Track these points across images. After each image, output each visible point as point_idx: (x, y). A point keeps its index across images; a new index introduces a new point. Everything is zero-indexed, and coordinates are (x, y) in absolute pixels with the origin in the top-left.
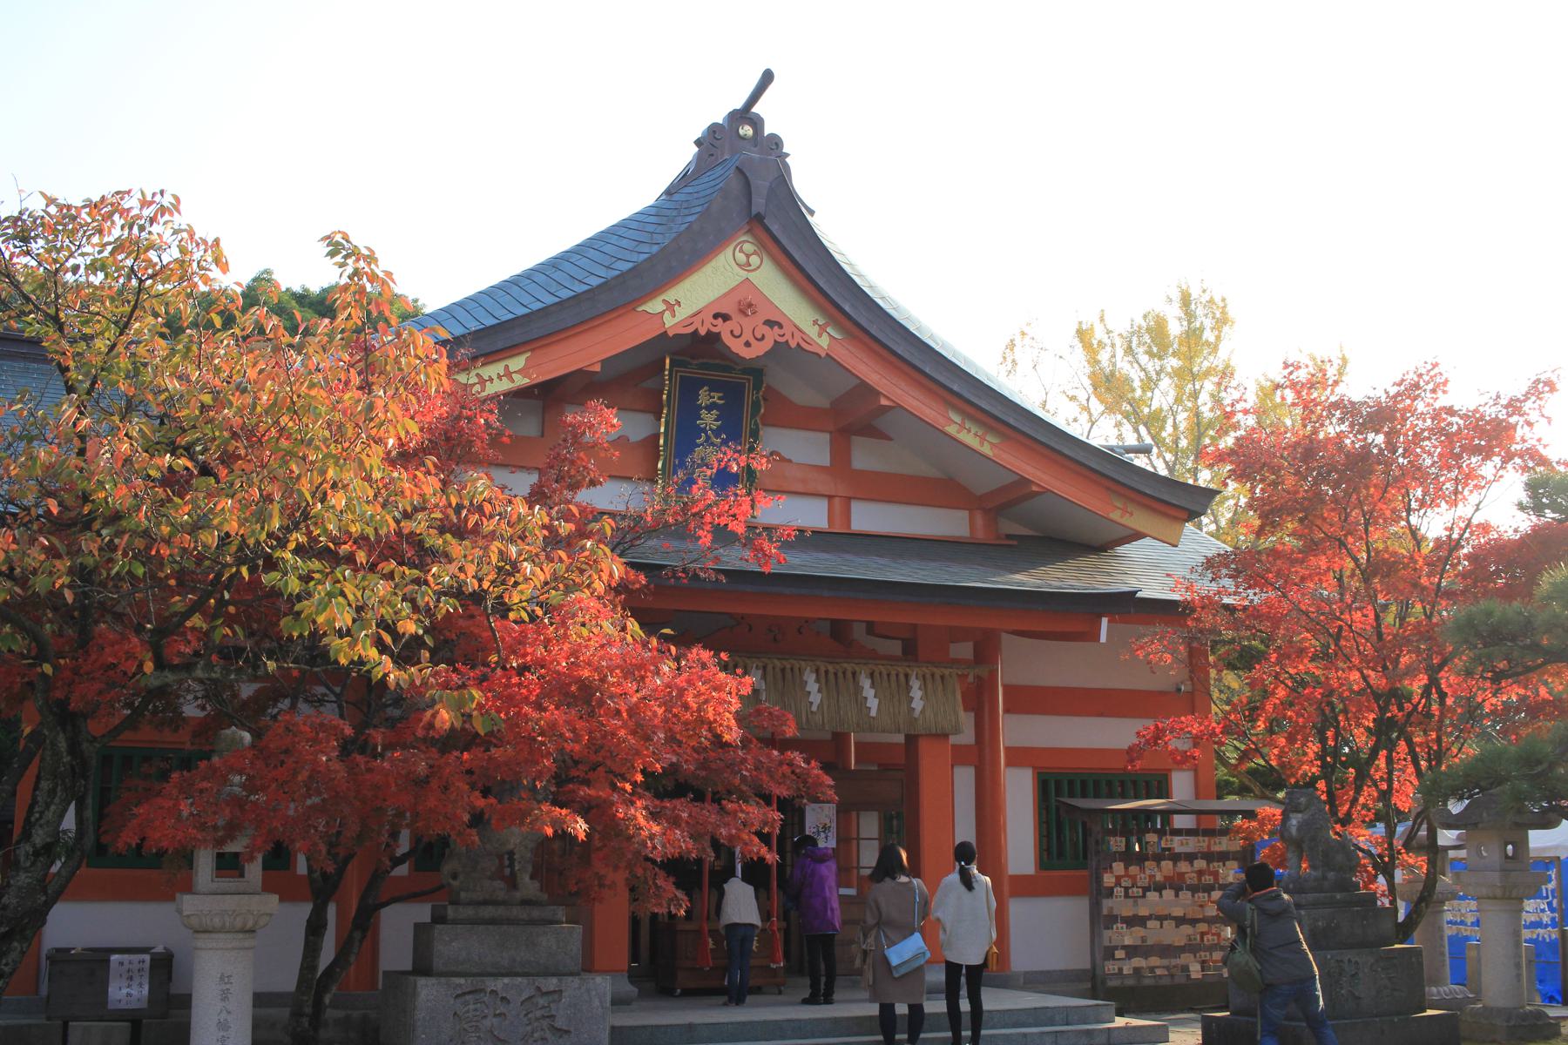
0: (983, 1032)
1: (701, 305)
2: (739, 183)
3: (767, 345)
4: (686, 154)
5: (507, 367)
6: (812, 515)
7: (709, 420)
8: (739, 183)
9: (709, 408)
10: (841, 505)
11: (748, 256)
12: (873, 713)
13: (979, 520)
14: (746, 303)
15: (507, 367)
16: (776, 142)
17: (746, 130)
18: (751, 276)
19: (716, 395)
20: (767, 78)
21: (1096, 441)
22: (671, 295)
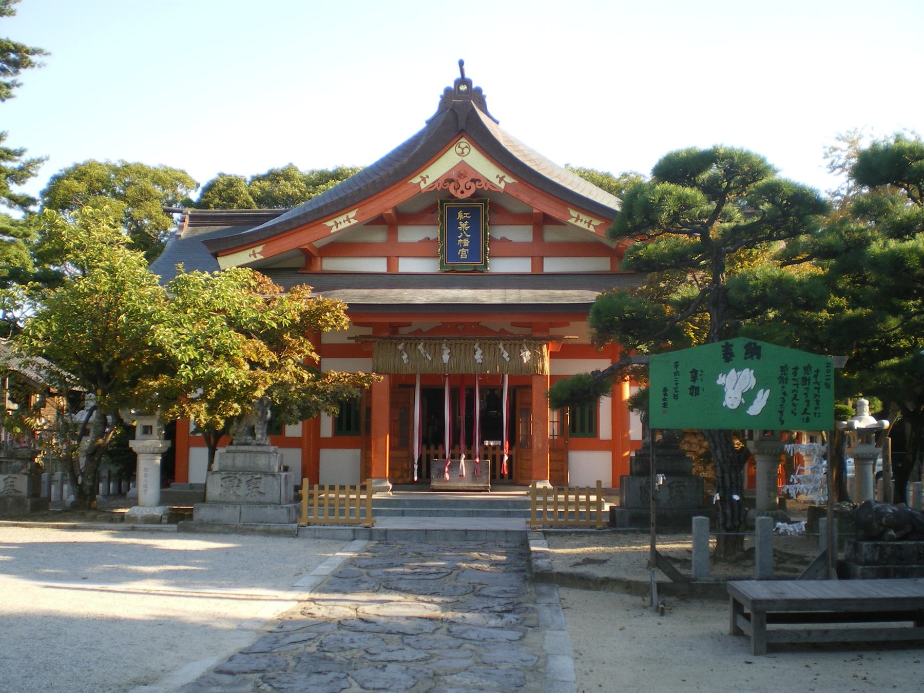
0: (649, 546)
1: (439, 176)
2: (461, 115)
3: (472, 191)
5: (504, 177)
6: (523, 266)
7: (464, 226)
8: (461, 115)
9: (463, 221)
10: (538, 261)
14: (463, 170)
15: (504, 177)
16: (479, 91)
17: (463, 88)
18: (464, 159)
20: (461, 63)
21: (339, 292)
22: (424, 174)
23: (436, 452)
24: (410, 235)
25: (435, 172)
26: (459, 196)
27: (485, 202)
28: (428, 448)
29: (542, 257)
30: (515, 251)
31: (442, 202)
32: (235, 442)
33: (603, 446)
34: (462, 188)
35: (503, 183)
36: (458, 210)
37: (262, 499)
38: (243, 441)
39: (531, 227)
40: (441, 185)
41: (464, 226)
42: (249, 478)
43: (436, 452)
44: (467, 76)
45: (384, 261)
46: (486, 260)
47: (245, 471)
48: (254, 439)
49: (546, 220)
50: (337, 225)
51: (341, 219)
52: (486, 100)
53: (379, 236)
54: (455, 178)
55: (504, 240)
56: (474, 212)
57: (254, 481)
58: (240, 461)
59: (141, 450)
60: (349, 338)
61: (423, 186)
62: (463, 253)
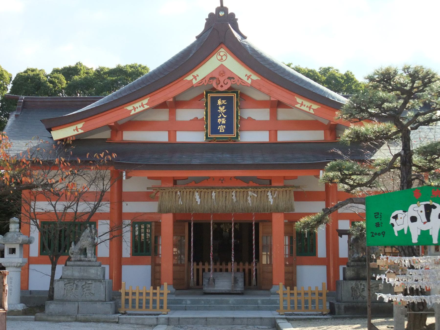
2: (220, 31)
4: (200, 28)
6: (262, 137)
7: (222, 109)
8: (220, 31)
9: (222, 106)
10: (274, 133)
11: (222, 56)
12: (272, 203)
13: (328, 132)
14: (222, 70)
16: (233, 15)
17: (221, 14)
18: (224, 63)
19: (224, 101)
22: (195, 73)
23: (221, 267)
24: (184, 115)
25: (203, 72)
26: (219, 89)
27: (237, 92)
28: (198, 264)
29: (276, 131)
30: (258, 126)
31: (207, 93)
32: (73, 259)
33: (321, 262)
34: (222, 83)
35: (250, 80)
36: (218, 98)
37: (93, 298)
38: (79, 259)
39: (268, 110)
40: (207, 81)
41: (222, 109)
42: (84, 283)
43: (221, 267)
44: (225, 5)
45: (167, 133)
46: (237, 133)
47: (81, 279)
48: (86, 257)
49: (279, 104)
50: (135, 109)
51: (137, 105)
52: (238, 22)
53: (163, 116)
54: (217, 76)
55: (249, 118)
56: (229, 100)
57: (87, 285)
58: (76, 273)
59: (8, 264)
60: (148, 188)
61: (194, 82)
62: (222, 128)
